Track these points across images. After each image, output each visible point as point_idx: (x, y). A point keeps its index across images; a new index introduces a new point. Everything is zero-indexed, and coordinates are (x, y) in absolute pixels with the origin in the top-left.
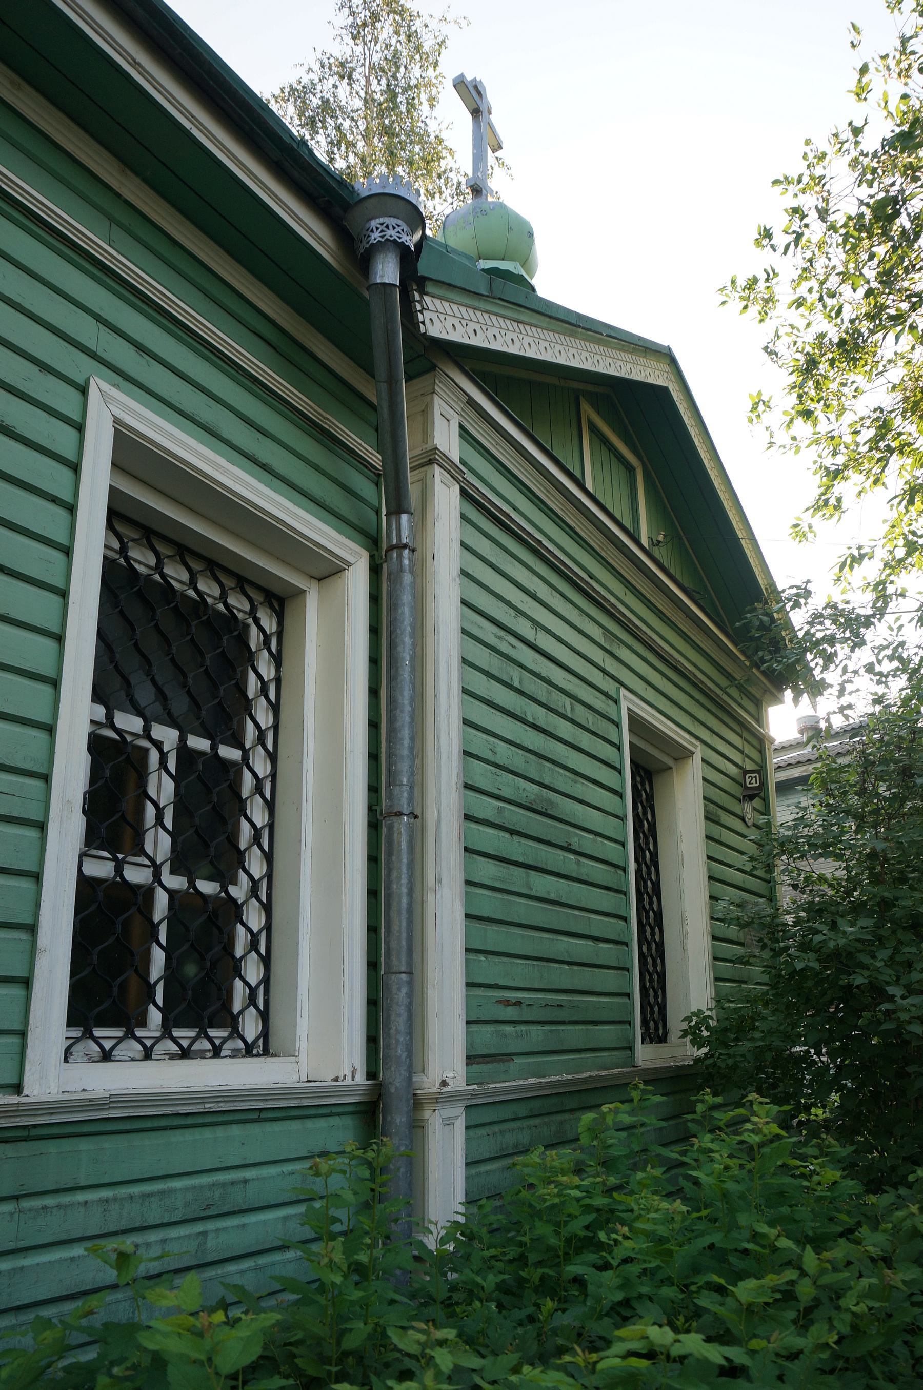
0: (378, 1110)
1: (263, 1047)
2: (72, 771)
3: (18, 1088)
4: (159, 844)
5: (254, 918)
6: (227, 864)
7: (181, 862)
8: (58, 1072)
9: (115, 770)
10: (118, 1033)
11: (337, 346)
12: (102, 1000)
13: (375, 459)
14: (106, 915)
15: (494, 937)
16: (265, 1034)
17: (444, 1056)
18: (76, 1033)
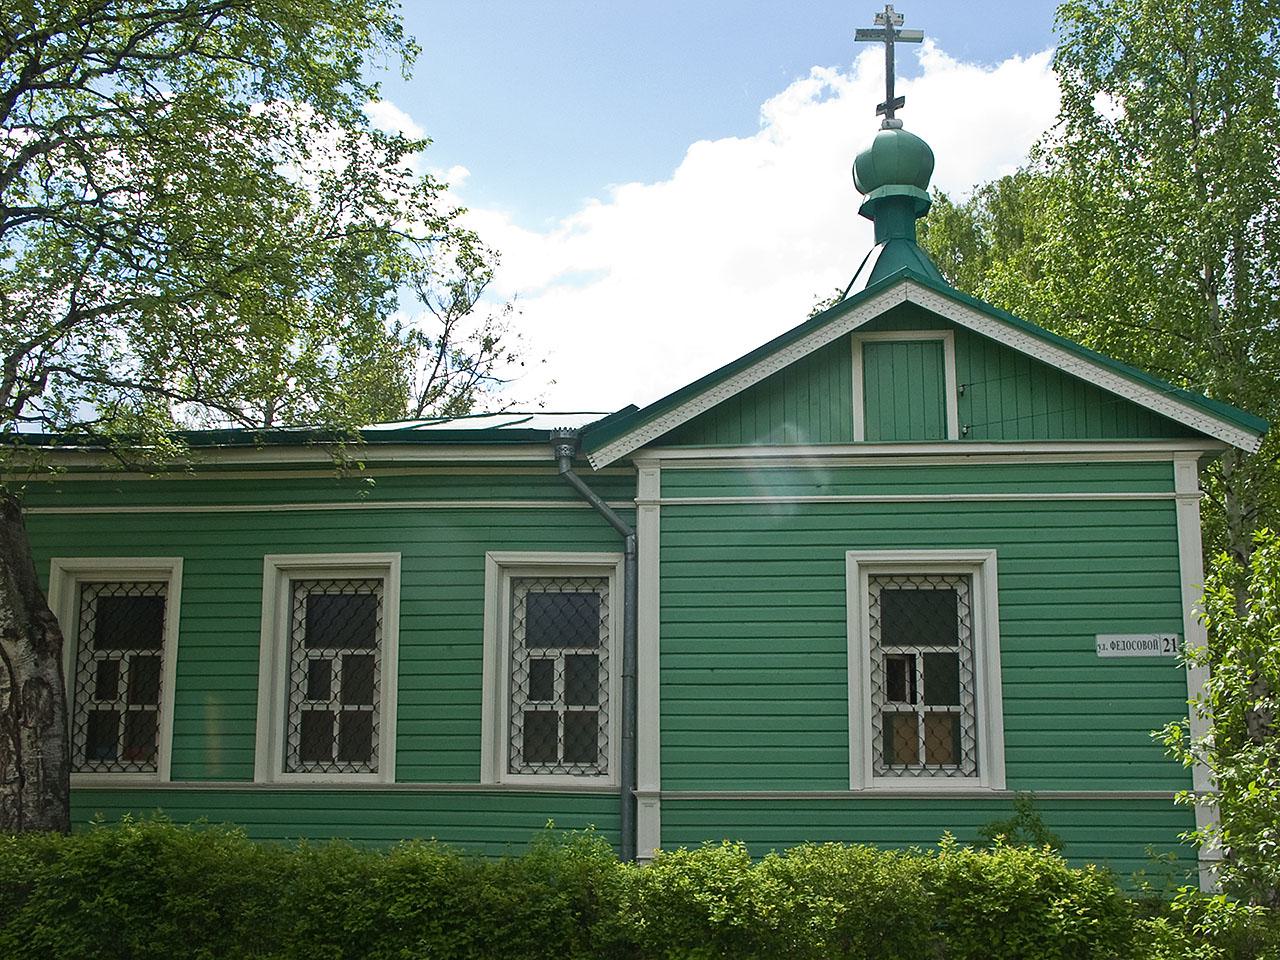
0: (626, 801)
7: (132, 700)
13: (586, 505)
17: (649, 781)
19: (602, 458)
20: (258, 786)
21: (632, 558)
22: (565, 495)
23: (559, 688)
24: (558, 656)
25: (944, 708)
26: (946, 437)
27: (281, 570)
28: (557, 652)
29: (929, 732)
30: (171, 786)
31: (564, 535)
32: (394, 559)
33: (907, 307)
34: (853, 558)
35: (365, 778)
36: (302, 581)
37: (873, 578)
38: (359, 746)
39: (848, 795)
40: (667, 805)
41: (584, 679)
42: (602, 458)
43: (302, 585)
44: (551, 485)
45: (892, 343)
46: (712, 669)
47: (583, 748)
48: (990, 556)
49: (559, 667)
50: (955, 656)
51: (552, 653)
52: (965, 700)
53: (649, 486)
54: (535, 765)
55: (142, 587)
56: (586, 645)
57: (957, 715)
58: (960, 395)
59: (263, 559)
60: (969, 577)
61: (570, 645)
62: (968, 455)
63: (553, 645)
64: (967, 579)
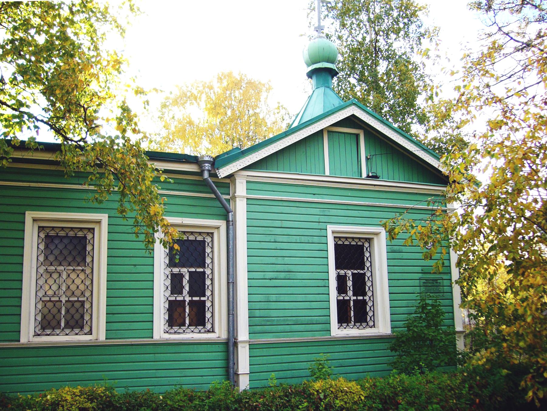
0: (230, 346)
1: (90, 333)
2: (333, 284)
3: (152, 338)
4: (350, 293)
5: (370, 304)
6: (364, 294)
7: (191, 294)
8: (337, 331)
9: (341, 281)
10: (194, 327)
11: (31, 163)
12: (343, 319)
13: (213, 196)
14: (342, 306)
15: (396, 303)
16: (374, 325)
17: (243, 334)
18: (340, 325)
19: (223, 172)
20: (23, 344)
21: (230, 225)
22: (188, 189)
26: (361, 176)
27: (35, 220)
30: (106, 342)
31: (192, 210)
32: (104, 218)
33: (353, 116)
36: (43, 227)
39: (331, 338)
40: (252, 347)
41: (199, 284)
42: (223, 172)
43: (43, 229)
44: (187, 184)
46: (270, 279)
47: (199, 318)
51: (184, 270)
52: (208, 293)
53: (241, 188)
56: (199, 267)
58: (367, 159)
59: (25, 214)
61: (191, 266)
62: (375, 185)
63: (183, 266)
64: (369, 240)
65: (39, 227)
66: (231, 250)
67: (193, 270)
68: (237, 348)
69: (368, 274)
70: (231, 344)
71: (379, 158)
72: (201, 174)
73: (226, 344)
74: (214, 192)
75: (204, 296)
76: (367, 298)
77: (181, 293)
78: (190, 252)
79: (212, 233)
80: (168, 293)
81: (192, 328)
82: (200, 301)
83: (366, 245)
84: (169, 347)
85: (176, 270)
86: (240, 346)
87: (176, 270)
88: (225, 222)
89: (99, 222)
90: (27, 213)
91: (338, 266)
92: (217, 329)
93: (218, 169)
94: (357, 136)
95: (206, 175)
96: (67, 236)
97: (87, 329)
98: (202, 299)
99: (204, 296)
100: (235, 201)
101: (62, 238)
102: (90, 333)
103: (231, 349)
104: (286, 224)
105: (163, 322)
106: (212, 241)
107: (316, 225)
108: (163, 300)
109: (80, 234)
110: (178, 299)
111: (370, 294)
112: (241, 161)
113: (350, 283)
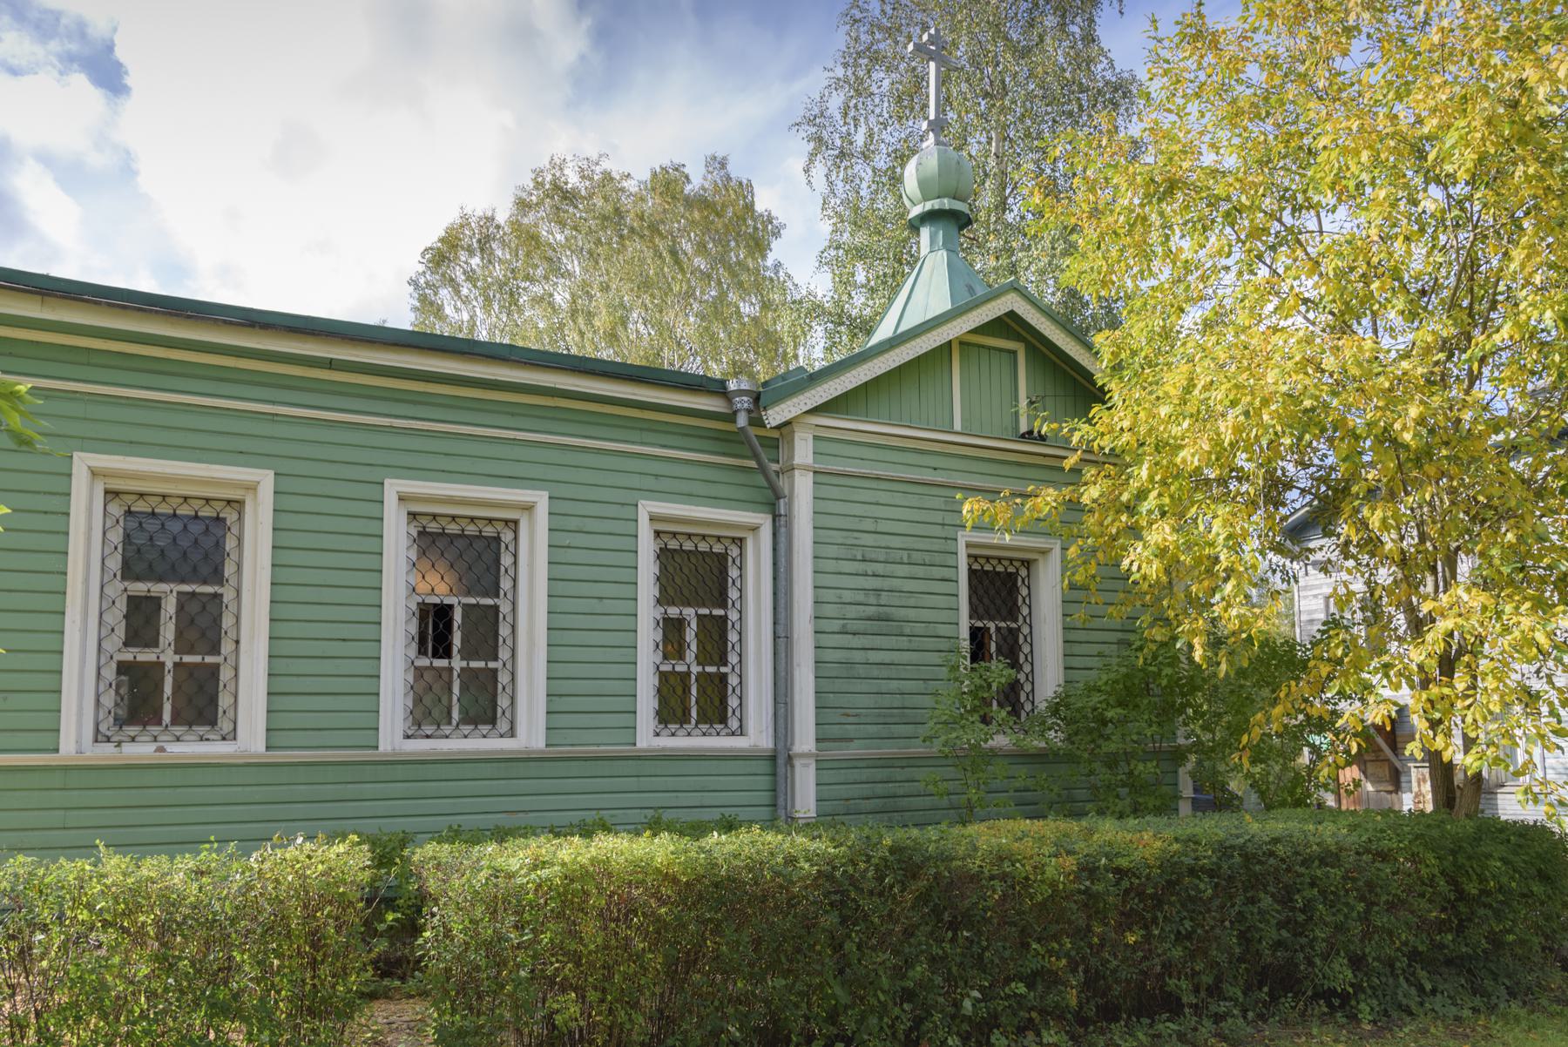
0: (777, 762)
2: (647, 635)
3: (57, 750)
5: (1028, 687)
10: (185, 728)
13: (753, 464)
17: (805, 739)
19: (775, 416)
20: (386, 755)
23: (168, 632)
24: (169, 594)
25: (481, 664)
27: (94, 473)
28: (164, 587)
29: (464, 688)
33: (1012, 314)
34: (82, 462)
35: (216, 749)
37: (413, 516)
38: (202, 703)
41: (716, 640)
44: (701, 437)
45: (989, 348)
47: (716, 706)
48: (541, 499)
49: (169, 607)
50: (496, 608)
51: (689, 612)
52: (504, 654)
53: (803, 450)
54: (673, 727)
55: (175, 502)
56: (486, 594)
57: (495, 671)
60: (241, 503)
61: (183, 581)
65: (107, 492)
66: (782, 576)
67: (705, 611)
68: (792, 766)
69: (1025, 630)
70: (781, 761)
71: (1049, 402)
72: (731, 417)
73: (773, 758)
74: (756, 457)
75: (496, 659)
76: (1022, 677)
77: (681, 657)
78: (698, 574)
79: (516, 522)
80: (658, 658)
81: (704, 727)
82: (487, 669)
83: (1023, 572)
84: (692, 767)
85: (673, 611)
86: (798, 763)
87: (673, 611)
88: (770, 517)
89: (529, 508)
90: (387, 482)
91: (974, 613)
92: (521, 728)
93: (765, 409)
94: (1014, 353)
95: (742, 420)
96: (462, 536)
97: (503, 725)
98: (492, 665)
99: (496, 659)
100: (792, 477)
101: (471, 539)
102: (512, 733)
103: (781, 770)
104: (883, 527)
105: (400, 714)
106: (516, 538)
107: (937, 531)
108: (401, 665)
109: (489, 531)
110: (678, 669)
111: (1027, 668)
112: (807, 394)
113: (690, 635)
